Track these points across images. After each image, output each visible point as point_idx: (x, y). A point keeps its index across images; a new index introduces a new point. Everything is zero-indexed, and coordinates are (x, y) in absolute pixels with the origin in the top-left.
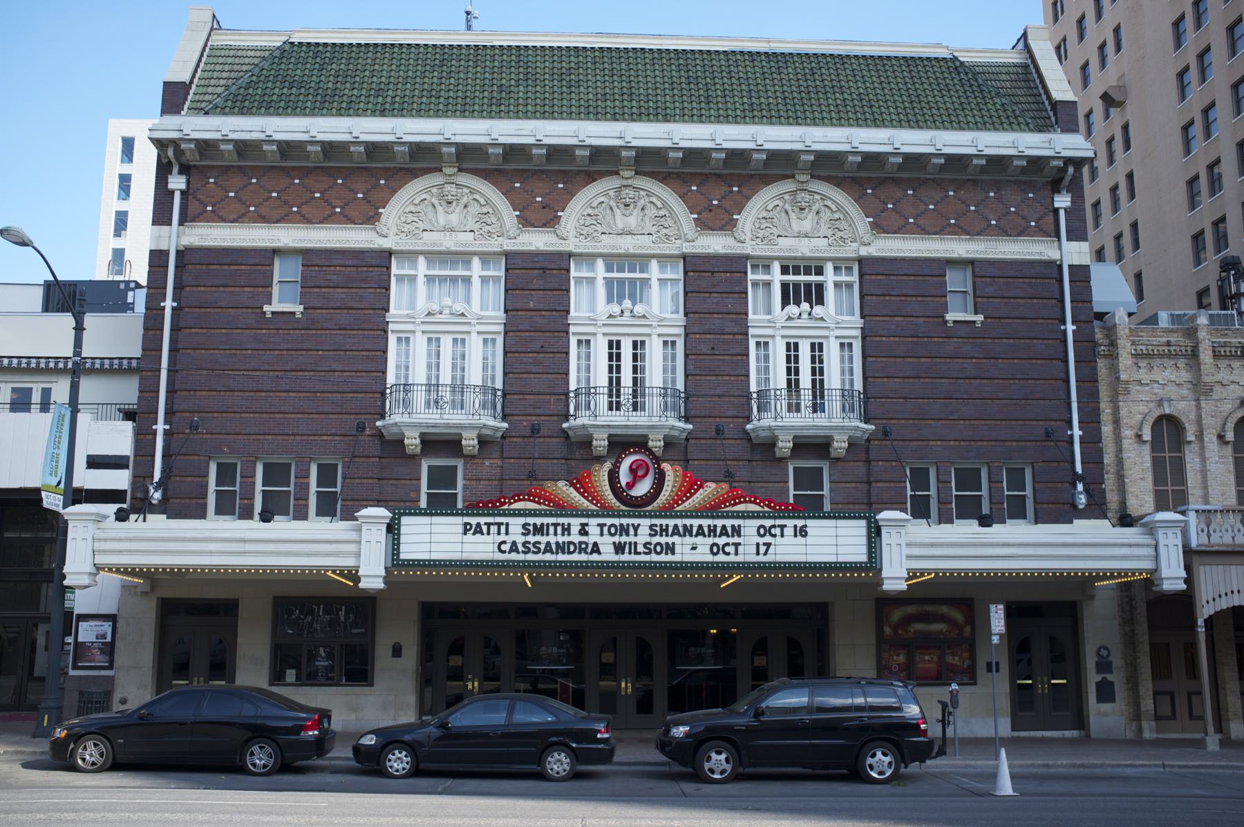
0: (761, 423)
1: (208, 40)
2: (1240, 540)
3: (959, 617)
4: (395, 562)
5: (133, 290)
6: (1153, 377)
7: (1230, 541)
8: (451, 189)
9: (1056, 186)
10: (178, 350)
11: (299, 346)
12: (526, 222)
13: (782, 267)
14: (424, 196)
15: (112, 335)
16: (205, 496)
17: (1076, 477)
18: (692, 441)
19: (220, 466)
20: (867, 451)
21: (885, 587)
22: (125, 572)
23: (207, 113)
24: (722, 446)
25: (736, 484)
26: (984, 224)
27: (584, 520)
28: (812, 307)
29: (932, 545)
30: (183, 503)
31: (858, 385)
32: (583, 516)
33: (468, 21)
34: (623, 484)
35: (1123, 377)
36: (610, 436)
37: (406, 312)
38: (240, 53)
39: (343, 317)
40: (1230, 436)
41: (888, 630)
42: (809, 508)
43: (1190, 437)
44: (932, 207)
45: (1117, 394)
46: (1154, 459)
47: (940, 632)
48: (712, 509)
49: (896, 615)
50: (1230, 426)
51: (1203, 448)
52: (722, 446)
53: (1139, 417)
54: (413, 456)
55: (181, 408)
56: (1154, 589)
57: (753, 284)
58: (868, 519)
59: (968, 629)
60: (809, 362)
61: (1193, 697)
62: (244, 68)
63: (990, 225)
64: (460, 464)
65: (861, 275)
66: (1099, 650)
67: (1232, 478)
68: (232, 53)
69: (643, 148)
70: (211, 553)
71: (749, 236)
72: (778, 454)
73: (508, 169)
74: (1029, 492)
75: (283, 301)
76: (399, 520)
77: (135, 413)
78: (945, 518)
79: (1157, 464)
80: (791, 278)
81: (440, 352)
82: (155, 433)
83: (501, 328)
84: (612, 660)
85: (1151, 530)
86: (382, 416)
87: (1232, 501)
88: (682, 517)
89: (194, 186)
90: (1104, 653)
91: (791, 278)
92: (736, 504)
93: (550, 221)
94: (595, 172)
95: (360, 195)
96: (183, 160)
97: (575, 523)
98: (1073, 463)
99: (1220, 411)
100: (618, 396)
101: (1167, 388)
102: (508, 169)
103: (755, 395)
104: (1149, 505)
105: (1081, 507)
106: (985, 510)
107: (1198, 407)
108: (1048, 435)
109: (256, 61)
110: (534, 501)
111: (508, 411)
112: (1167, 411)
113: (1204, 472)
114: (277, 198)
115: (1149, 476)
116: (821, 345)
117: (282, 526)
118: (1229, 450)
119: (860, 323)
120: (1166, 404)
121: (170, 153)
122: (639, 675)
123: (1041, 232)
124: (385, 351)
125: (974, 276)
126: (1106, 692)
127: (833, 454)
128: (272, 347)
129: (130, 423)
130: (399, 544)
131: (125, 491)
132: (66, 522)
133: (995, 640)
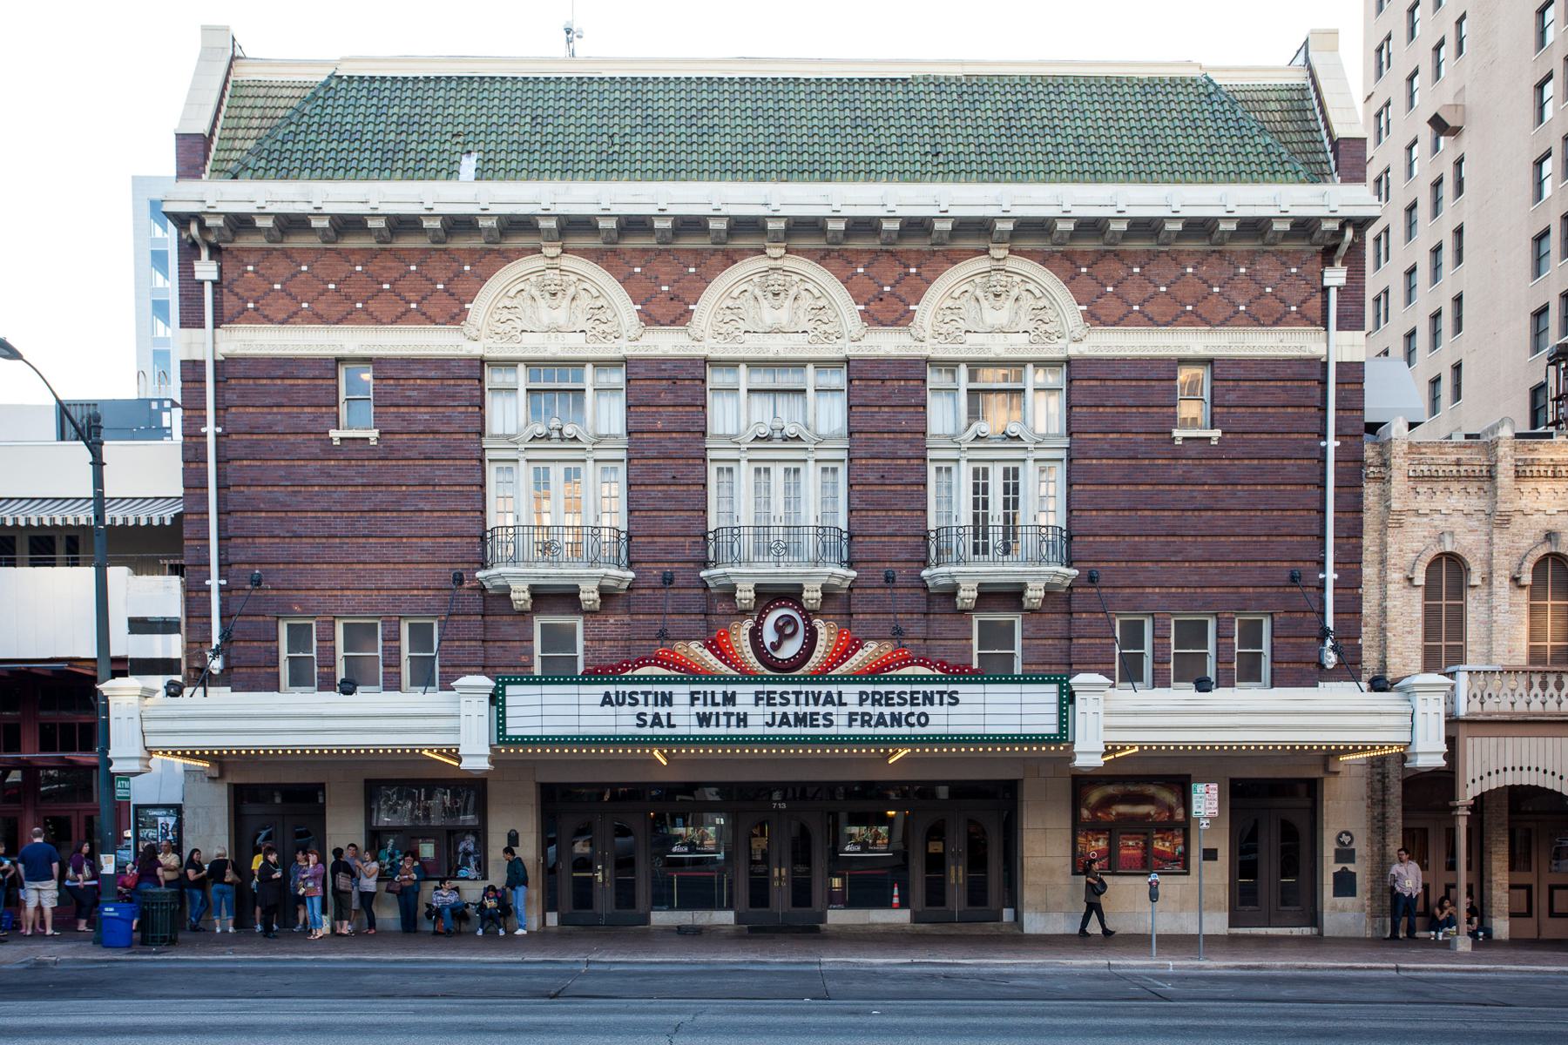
1: (228, 73)
4: (501, 737)
5: (169, 410)
7: (1508, 708)
9: (1328, 256)
10: (228, 487)
12: (649, 319)
14: (521, 286)
16: (276, 664)
17: (1324, 633)
18: (856, 591)
20: (1069, 601)
21: (1077, 763)
22: (193, 756)
23: (235, 177)
24: (894, 595)
25: (906, 642)
29: (1136, 714)
30: (249, 669)
33: (569, 41)
34: (768, 645)
35: (1395, 506)
36: (757, 586)
38: (273, 92)
39: (428, 443)
41: (1085, 813)
42: (996, 672)
43: (1475, 580)
45: (1386, 527)
46: (1426, 608)
47: (1148, 815)
49: (1095, 796)
50: (1528, 565)
51: (1490, 594)
52: (894, 595)
53: (1412, 556)
54: (522, 613)
61: (1556, 892)
62: (281, 113)
63: (1237, 312)
64: (579, 622)
68: (262, 92)
71: (929, 332)
72: (517, 606)
73: (618, 243)
74: (1266, 648)
76: (503, 689)
78: (1160, 681)
79: (1431, 614)
82: (208, 590)
84: (940, 850)
89: (230, 274)
90: (1346, 839)
93: (680, 318)
94: (735, 251)
98: (1323, 613)
99: (1519, 546)
100: (986, 536)
101: (1452, 519)
102: (618, 243)
103: (933, 534)
105: (1330, 666)
107: (1490, 543)
108: (1294, 579)
109: (296, 103)
110: (661, 666)
111: (634, 557)
112: (1448, 549)
113: (1489, 624)
114: (337, 291)
115: (1419, 629)
116: (1016, 470)
117: (368, 700)
120: (1448, 539)
121: (194, 229)
122: (795, 861)
123: (1305, 319)
126: (1345, 884)
127: (1026, 605)
129: (177, 578)
130: (504, 718)
131: (179, 660)
132: (106, 699)
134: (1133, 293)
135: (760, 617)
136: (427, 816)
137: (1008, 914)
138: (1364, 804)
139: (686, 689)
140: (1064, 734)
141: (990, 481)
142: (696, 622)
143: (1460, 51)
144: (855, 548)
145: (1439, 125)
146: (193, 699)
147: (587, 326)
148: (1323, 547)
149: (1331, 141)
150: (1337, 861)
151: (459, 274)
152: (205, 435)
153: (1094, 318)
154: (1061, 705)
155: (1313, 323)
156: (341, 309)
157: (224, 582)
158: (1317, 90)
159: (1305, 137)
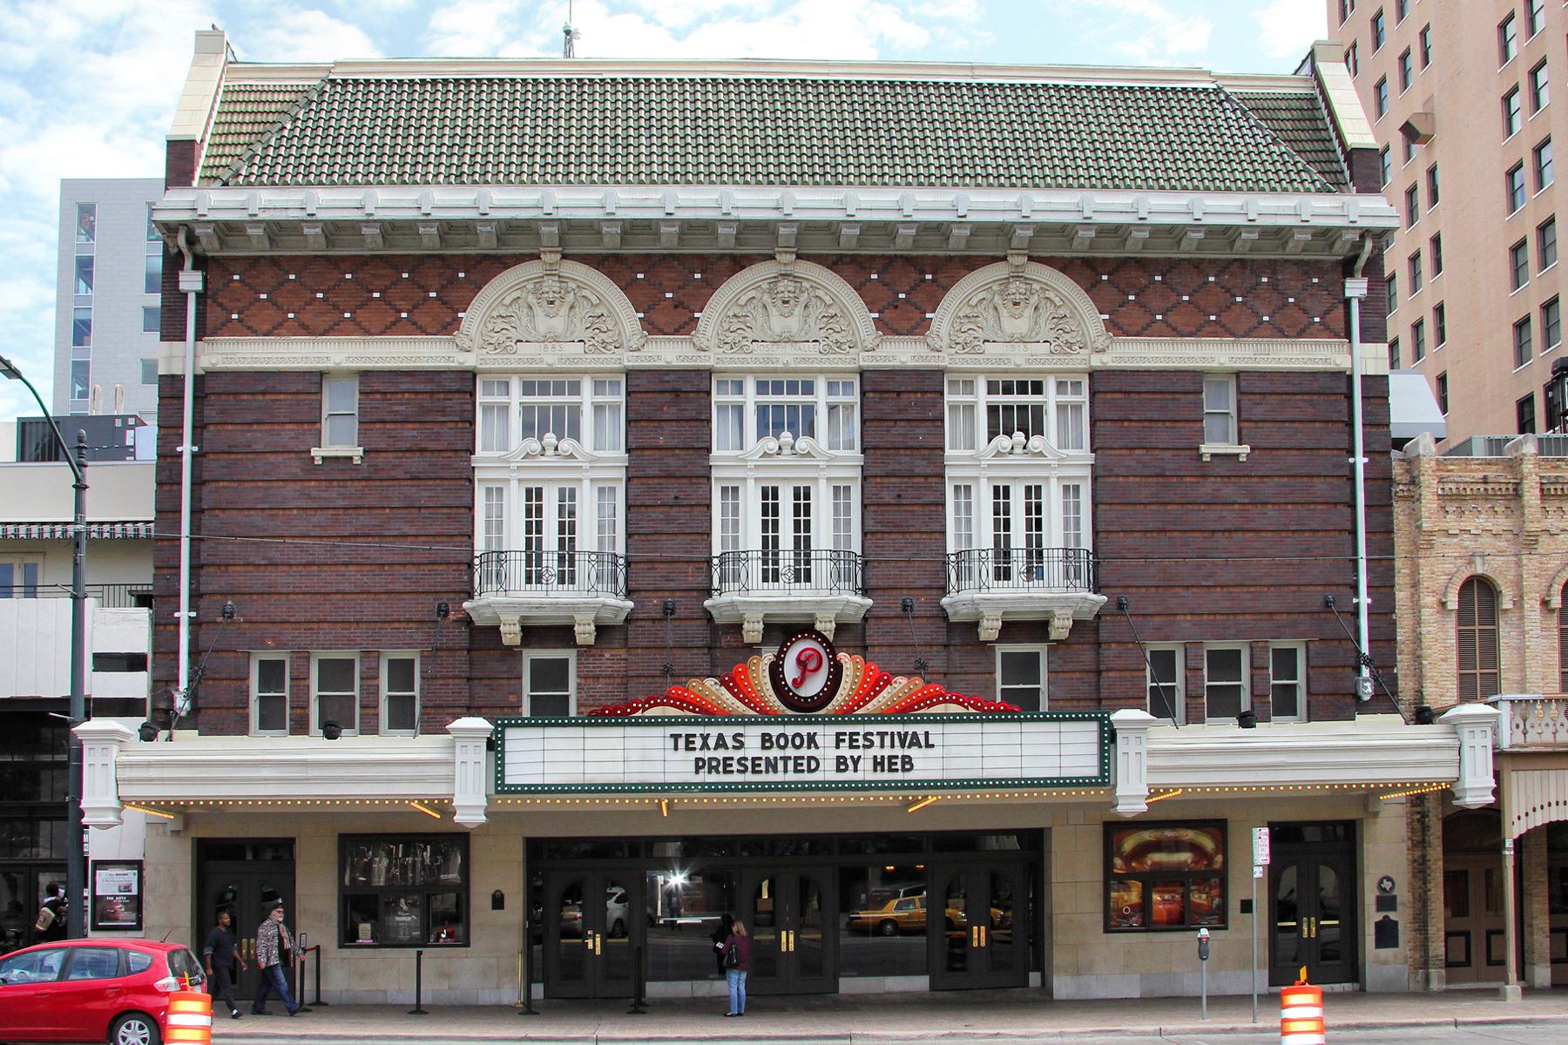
0: (960, 598)
2: (1562, 737)
3: (1208, 844)
4: (500, 786)
5: (132, 427)
6: (1463, 526)
8: (551, 284)
9: (1347, 267)
11: (359, 503)
12: (652, 327)
13: (989, 383)
14: (518, 293)
15: (123, 495)
16: (246, 706)
19: (393, 664)
20: (1097, 630)
23: (226, 184)
26: (1253, 322)
27: (739, 730)
28: (1027, 438)
30: (216, 713)
31: (1087, 543)
32: (737, 723)
34: (789, 683)
35: (1426, 526)
37: (496, 454)
39: (417, 463)
40: (1556, 602)
41: (1118, 862)
43: (1506, 603)
44: (1186, 298)
48: (903, 712)
49: (1129, 844)
51: (1522, 618)
55: (211, 588)
56: (1455, 803)
57: (719, 408)
58: (1101, 721)
59: (1219, 858)
60: (1023, 515)
61: (1493, 937)
64: (570, 655)
65: (1093, 394)
66: (1381, 882)
67: (1556, 656)
68: (257, 97)
69: (807, 222)
70: (266, 780)
71: (946, 341)
72: (506, 640)
74: (1301, 680)
75: (339, 440)
76: (503, 733)
77: (151, 597)
78: (1194, 717)
79: (1464, 639)
80: (771, 398)
81: (544, 511)
82: (177, 623)
83: (622, 474)
85: (1454, 727)
86: (470, 595)
87: (1554, 688)
88: (863, 722)
91: (771, 398)
92: (933, 704)
93: (919, 327)
94: (743, 256)
95: (433, 295)
96: (198, 249)
97: (729, 732)
100: (776, 562)
104: (1452, 694)
105: (1366, 698)
106: (1245, 706)
107: (1519, 564)
111: (633, 585)
112: (1480, 571)
113: (1521, 650)
115: (1453, 657)
117: (352, 746)
118: (1554, 621)
119: (1089, 458)
120: (1478, 560)
121: (181, 240)
123: (1327, 331)
124: (471, 508)
125: (1240, 392)
128: (323, 504)
129: (146, 609)
130: (503, 765)
131: (144, 700)
133: (1258, 872)
134: (1156, 303)
135: (781, 652)
136: (404, 875)
137: (1034, 978)
138: (1404, 846)
139: (832, 730)
140: (1105, 777)
141: (544, 503)
142: (701, 659)
143: (1426, 61)
144: (869, 574)
145: (1410, 133)
146: (161, 748)
147: (586, 335)
148: (1356, 570)
149: (1344, 150)
150: (1379, 909)
151: (453, 281)
152: (180, 455)
153: (1116, 327)
154: (1101, 745)
155: (1337, 336)
156: (328, 319)
157: (194, 614)
158: (1326, 100)
159: (1318, 146)
